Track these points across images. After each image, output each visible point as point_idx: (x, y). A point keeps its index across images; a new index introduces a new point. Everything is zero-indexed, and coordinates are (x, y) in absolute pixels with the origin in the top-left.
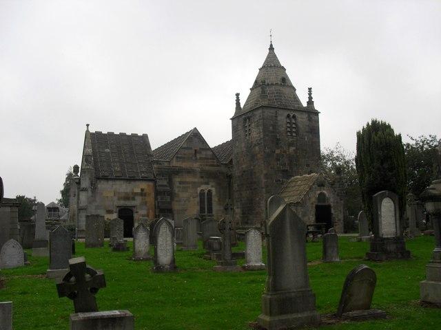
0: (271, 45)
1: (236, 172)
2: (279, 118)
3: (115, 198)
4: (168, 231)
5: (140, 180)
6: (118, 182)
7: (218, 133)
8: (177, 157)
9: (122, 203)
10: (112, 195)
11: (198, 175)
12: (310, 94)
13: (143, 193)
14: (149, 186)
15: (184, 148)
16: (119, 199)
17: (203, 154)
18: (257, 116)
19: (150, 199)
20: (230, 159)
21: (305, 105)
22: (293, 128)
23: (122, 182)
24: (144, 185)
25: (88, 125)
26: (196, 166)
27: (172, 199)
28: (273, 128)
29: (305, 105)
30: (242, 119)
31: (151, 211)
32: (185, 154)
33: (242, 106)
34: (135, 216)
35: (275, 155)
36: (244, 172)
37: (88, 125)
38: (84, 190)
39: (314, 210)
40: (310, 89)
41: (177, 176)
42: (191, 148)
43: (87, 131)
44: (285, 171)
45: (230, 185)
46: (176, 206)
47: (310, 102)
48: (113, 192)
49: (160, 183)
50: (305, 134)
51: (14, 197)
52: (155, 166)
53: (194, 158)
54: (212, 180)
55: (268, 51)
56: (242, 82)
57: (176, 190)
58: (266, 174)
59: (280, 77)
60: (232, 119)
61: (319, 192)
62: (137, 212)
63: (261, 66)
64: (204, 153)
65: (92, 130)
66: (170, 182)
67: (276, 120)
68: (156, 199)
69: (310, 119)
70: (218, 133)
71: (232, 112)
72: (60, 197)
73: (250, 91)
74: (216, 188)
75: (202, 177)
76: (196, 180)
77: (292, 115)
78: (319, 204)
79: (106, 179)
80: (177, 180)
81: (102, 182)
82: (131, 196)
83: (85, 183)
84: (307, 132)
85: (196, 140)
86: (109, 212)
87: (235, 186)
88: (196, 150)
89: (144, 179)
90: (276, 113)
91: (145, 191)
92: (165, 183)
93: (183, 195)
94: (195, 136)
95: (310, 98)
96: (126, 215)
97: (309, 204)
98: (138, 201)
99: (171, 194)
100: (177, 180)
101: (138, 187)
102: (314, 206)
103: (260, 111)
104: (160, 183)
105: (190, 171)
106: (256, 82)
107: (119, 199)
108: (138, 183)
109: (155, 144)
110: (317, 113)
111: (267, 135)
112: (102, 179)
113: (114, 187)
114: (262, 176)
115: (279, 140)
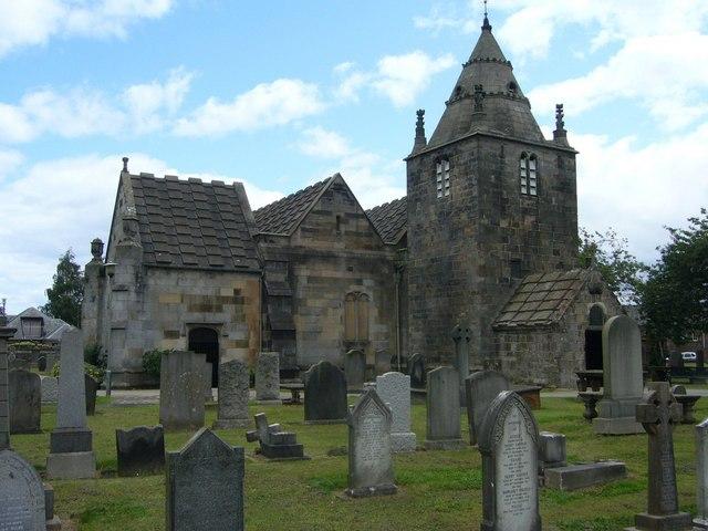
0: (486, 21)
1: (415, 260)
2: (506, 160)
3: (184, 308)
4: (524, 435)
6: (189, 275)
7: (379, 185)
8: (303, 230)
9: (197, 317)
10: (178, 301)
11: (344, 266)
13: (237, 299)
15: (318, 212)
16: (191, 309)
17: (352, 226)
19: (253, 308)
20: (402, 233)
21: (548, 135)
22: (526, 177)
24: (240, 282)
25: (125, 160)
26: (339, 247)
27: (294, 311)
28: (496, 178)
29: (548, 135)
32: (318, 224)
33: (429, 135)
34: (222, 342)
37: (125, 160)
38: (121, 289)
42: (328, 213)
43: (125, 170)
44: (515, 263)
45: (402, 287)
46: (301, 324)
47: (560, 132)
48: (178, 295)
49: (271, 277)
50: (552, 192)
51: (210, 182)
53: (334, 232)
54: (368, 275)
57: (301, 294)
58: (484, 267)
60: (409, 160)
61: (591, 305)
64: (353, 222)
67: (502, 163)
68: (264, 310)
69: (560, 165)
70: (379, 185)
71: (408, 147)
72: (46, 300)
74: (374, 291)
75: (350, 269)
76: (339, 275)
78: (592, 328)
79: (166, 268)
80: (303, 272)
81: (157, 273)
83: (125, 276)
85: (338, 197)
86: (171, 334)
87: (412, 288)
88: (338, 217)
89: (242, 271)
90: (494, 153)
92: (281, 277)
93: (315, 303)
94: (337, 189)
95: (560, 124)
96: (204, 341)
97: (574, 328)
98: (227, 315)
99: (291, 300)
100: (303, 272)
101: (228, 286)
103: (473, 144)
104: (271, 277)
105: (328, 257)
106: (458, 89)
107: (191, 309)
108: (228, 277)
109: (258, 199)
110: (572, 154)
111: (487, 192)
115: (507, 201)
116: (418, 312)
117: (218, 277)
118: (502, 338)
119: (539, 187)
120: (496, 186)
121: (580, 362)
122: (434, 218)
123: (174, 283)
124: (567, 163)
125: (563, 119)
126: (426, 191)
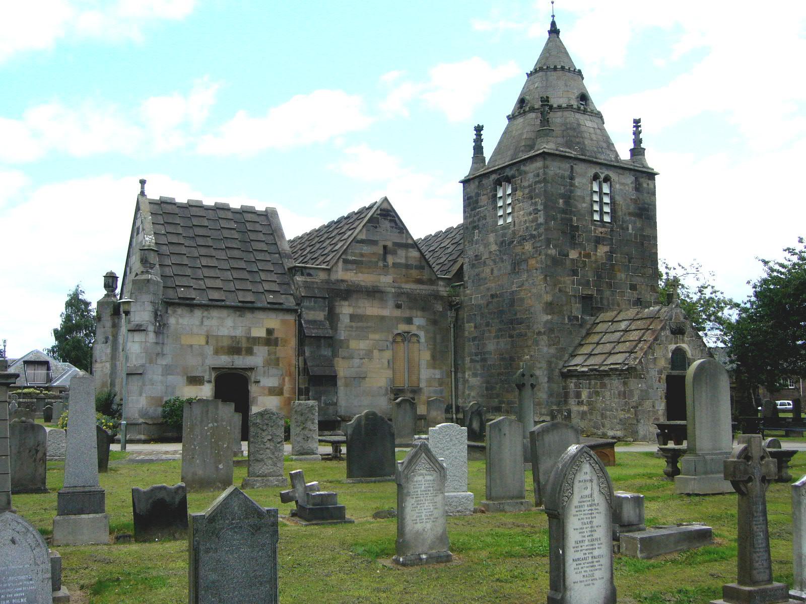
0: (553, 24)
2: (577, 182)
3: (209, 350)
5: (263, 309)
6: (215, 313)
7: (432, 209)
9: (224, 360)
10: (202, 341)
12: (637, 133)
13: (270, 340)
14: (284, 322)
15: (362, 242)
16: (217, 352)
17: (401, 257)
18: (531, 175)
19: (288, 351)
20: (457, 267)
21: (625, 155)
23: (225, 313)
24: (273, 321)
25: (143, 182)
26: (385, 280)
27: (335, 355)
29: (625, 155)
30: (483, 183)
31: (287, 379)
32: (362, 255)
33: (488, 153)
35: (568, 262)
36: (492, 296)
37: (143, 182)
39: (663, 386)
40: (637, 122)
41: (346, 303)
42: (374, 243)
45: (458, 326)
46: (343, 369)
47: (637, 151)
48: (203, 334)
52: (299, 278)
53: (381, 264)
54: (419, 313)
55: (547, 36)
56: (485, 98)
57: (342, 335)
58: (551, 303)
59: (577, 93)
60: (466, 182)
61: (673, 347)
62: (257, 382)
63: (531, 68)
64: (401, 252)
65: (153, 193)
66: (332, 317)
67: (572, 185)
68: (300, 352)
69: (638, 188)
70: (432, 209)
71: (465, 168)
73: (507, 122)
74: (427, 332)
75: (398, 306)
76: (386, 312)
77: (602, 176)
78: (279, 339)
79: (189, 305)
80: (345, 310)
81: (179, 311)
82: (244, 344)
84: (630, 214)
85: (386, 224)
86: (195, 380)
87: (469, 327)
88: (385, 247)
89: (275, 308)
91: (276, 334)
92: (320, 316)
94: (384, 215)
95: (638, 141)
97: (653, 373)
98: (258, 358)
99: (331, 341)
100: (345, 310)
101: (259, 326)
102: (664, 376)
103: (539, 164)
105: (374, 293)
106: (522, 101)
107: (217, 352)
108: (260, 315)
109: (294, 226)
111: (554, 219)
112: (179, 305)
113: (206, 322)
114: (538, 307)
116: (476, 355)
117: (249, 315)
118: (572, 384)
119: (613, 213)
120: (564, 211)
121: (661, 412)
122: (494, 248)
123: (197, 323)
124: (645, 185)
125: (641, 136)
126: (485, 218)
